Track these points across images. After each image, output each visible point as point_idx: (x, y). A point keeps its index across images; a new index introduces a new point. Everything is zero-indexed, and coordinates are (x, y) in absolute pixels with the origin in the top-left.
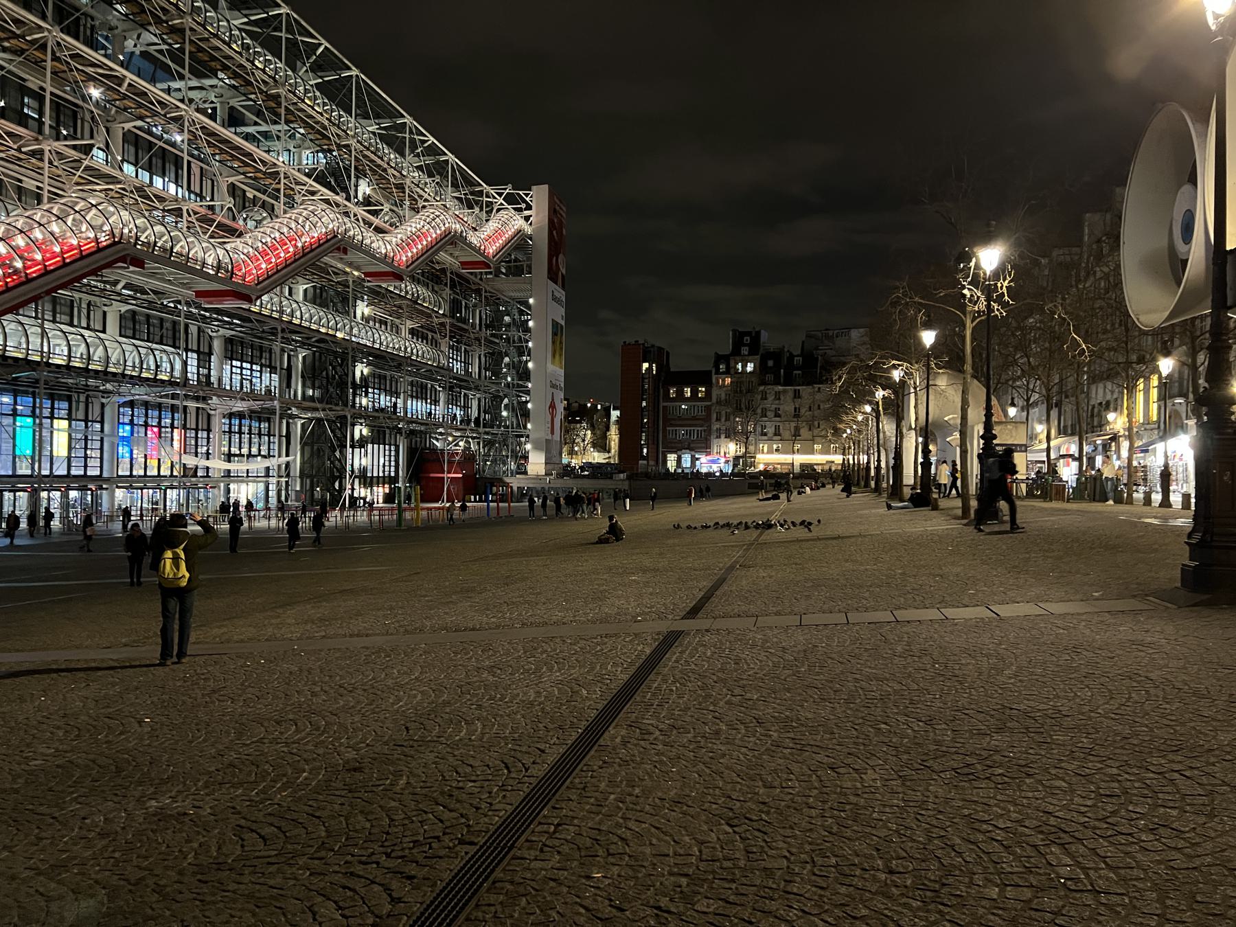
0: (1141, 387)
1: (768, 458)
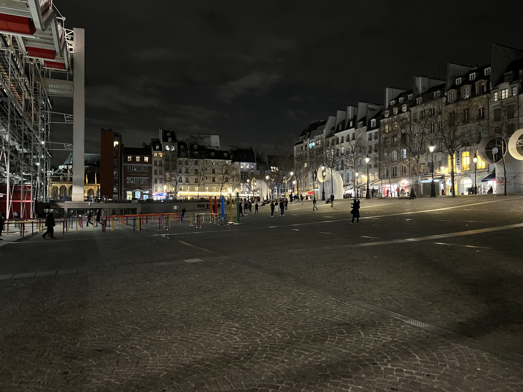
0: (450, 158)
1: (186, 193)
